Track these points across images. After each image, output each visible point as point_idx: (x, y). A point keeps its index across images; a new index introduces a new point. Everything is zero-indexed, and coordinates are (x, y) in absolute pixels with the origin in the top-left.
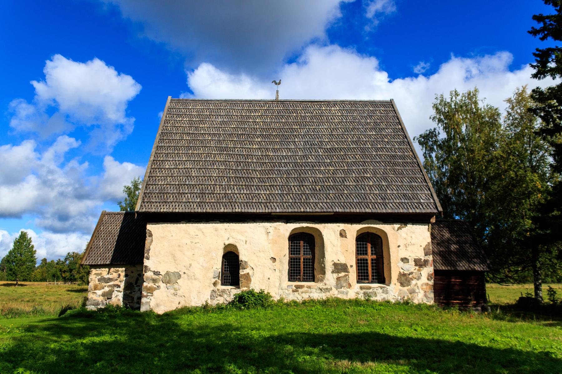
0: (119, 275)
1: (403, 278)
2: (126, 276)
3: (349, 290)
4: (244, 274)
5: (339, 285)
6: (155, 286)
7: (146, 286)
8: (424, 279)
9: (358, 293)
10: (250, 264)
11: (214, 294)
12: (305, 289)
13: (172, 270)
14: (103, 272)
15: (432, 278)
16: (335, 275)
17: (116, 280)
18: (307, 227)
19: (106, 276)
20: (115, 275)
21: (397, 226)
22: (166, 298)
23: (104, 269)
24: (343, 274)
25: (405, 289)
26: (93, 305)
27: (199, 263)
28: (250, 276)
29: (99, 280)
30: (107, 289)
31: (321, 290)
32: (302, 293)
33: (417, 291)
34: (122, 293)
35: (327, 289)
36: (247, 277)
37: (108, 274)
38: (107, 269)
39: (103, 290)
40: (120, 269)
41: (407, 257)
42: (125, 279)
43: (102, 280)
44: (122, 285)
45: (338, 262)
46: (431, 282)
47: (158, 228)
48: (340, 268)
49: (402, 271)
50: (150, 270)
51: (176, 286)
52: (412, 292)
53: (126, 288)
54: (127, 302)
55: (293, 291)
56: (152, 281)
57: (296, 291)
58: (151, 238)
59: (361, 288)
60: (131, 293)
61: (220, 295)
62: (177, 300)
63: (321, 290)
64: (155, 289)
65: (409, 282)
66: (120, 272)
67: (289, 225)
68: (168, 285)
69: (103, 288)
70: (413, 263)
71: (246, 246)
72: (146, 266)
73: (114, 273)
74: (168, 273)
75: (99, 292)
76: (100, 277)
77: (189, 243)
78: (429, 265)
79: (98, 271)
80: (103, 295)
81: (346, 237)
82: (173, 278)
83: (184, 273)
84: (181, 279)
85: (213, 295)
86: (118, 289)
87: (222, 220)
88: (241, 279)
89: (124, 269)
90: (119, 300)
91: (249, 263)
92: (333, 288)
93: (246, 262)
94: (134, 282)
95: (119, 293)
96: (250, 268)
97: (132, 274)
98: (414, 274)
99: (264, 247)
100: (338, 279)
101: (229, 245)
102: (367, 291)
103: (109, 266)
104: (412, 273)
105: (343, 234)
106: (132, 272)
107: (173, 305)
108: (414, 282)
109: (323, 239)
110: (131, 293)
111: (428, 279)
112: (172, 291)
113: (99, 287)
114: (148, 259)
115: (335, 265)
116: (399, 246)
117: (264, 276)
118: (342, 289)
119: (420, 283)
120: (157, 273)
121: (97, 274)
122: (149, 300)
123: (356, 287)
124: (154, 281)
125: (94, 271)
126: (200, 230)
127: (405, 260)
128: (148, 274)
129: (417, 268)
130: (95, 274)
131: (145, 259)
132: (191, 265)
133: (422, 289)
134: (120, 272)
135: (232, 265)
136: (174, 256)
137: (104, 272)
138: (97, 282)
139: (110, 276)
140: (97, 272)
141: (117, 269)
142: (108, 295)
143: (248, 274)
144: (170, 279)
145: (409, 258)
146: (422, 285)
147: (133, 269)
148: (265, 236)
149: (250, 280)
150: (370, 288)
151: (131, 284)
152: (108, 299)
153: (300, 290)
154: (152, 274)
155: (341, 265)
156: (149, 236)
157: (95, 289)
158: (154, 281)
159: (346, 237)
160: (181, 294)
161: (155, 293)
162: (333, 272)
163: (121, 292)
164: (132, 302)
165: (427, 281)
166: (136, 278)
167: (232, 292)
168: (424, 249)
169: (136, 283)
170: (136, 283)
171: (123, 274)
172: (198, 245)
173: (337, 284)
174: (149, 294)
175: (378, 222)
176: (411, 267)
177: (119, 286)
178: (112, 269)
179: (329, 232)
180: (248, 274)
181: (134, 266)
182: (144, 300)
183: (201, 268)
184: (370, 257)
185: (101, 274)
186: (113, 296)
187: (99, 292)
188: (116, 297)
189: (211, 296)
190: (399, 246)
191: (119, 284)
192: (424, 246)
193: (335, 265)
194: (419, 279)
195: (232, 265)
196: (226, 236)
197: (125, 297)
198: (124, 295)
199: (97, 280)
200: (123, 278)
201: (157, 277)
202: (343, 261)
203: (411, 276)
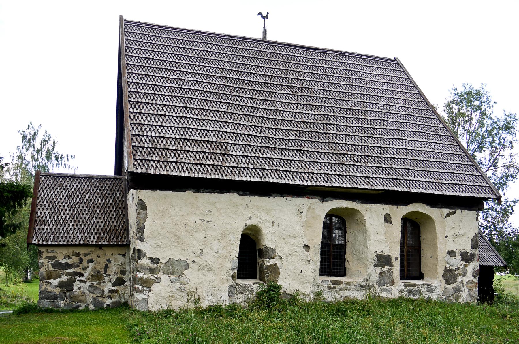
0: (81, 260)
1: (448, 275)
3: (392, 287)
4: (271, 265)
5: (381, 283)
6: (153, 278)
8: (469, 277)
9: (401, 291)
11: (232, 290)
12: (344, 285)
14: (57, 256)
15: (477, 275)
16: (378, 270)
17: (78, 266)
18: (347, 208)
21: (446, 211)
24: (386, 268)
25: (451, 287)
27: (212, 249)
29: (53, 266)
30: (65, 278)
31: (362, 287)
32: (340, 290)
33: (462, 289)
35: (369, 285)
36: (274, 269)
41: (454, 250)
43: (58, 265)
45: (382, 253)
46: (476, 280)
47: (306, 225)
48: (383, 260)
49: (448, 266)
50: (145, 256)
51: (183, 279)
52: (457, 290)
55: (330, 288)
56: (148, 271)
57: (334, 288)
58: (144, 212)
59: (406, 286)
60: (99, 284)
61: (241, 292)
64: (154, 282)
65: (454, 278)
67: (325, 203)
68: (172, 277)
69: (60, 277)
70: (460, 257)
71: (272, 229)
73: (73, 257)
75: (55, 282)
76: (54, 261)
77: (199, 221)
78: (476, 260)
80: (61, 285)
81: (391, 223)
82: (178, 268)
83: (194, 261)
84: (189, 270)
85: (232, 290)
87: (241, 193)
91: (277, 251)
92: (375, 285)
93: (273, 250)
94: (102, 270)
96: (278, 257)
97: (98, 260)
98: (460, 270)
99: (292, 232)
100: (381, 274)
101: (252, 226)
102: (411, 288)
104: (458, 269)
105: (388, 219)
106: (99, 257)
108: (460, 279)
110: (99, 284)
111: (473, 276)
113: (54, 275)
115: (379, 256)
116: (446, 237)
118: (385, 287)
119: (465, 280)
120: (155, 261)
121: (50, 258)
122: (146, 297)
123: (400, 284)
124: (152, 271)
127: (452, 253)
129: (464, 263)
130: (47, 257)
132: (202, 250)
133: (467, 287)
135: (251, 254)
136: (178, 238)
138: (51, 269)
143: (276, 264)
144: (175, 269)
145: (457, 251)
146: (467, 283)
149: (278, 273)
150: (415, 285)
152: (68, 291)
153: (338, 287)
154: (149, 261)
155: (384, 256)
158: (152, 271)
159: (391, 223)
162: (375, 266)
164: (102, 296)
165: (472, 278)
166: (104, 264)
168: (472, 241)
169: (105, 272)
172: (211, 224)
173: (380, 281)
174: (146, 289)
176: (457, 262)
179: (372, 214)
180: (276, 264)
184: (336, 234)
185: (55, 257)
187: (55, 282)
188: (79, 288)
189: (229, 293)
190: (446, 237)
192: (471, 238)
193: (379, 256)
194: (464, 275)
195: (251, 254)
196: (248, 214)
199: (50, 266)
201: (155, 266)
202: (387, 253)
203: (457, 272)
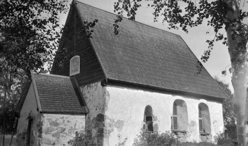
0: (64, 121)
138: (49, 126)
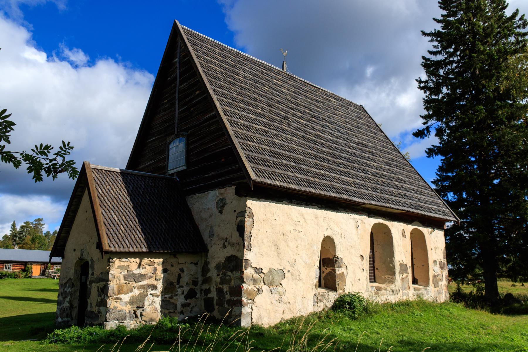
2: (165, 271)
7: (247, 289)
10: (346, 261)
13: (276, 267)
16: (401, 276)
17: (151, 277)
19: (137, 271)
20: (147, 270)
22: (269, 307)
23: (132, 260)
26: (117, 320)
28: (344, 276)
29: (125, 277)
30: (137, 292)
34: (160, 298)
37: (139, 267)
38: (138, 260)
39: (131, 294)
40: (157, 260)
42: (162, 275)
44: (160, 286)
48: (403, 268)
53: (165, 291)
54: (167, 311)
60: (171, 298)
62: (281, 307)
63: (393, 291)
66: (156, 265)
69: (131, 291)
72: (247, 260)
73: (147, 267)
74: (271, 271)
75: (126, 298)
76: (126, 272)
79: (125, 262)
82: (277, 278)
83: (289, 271)
84: (285, 279)
85: (317, 299)
86: (153, 292)
88: (337, 280)
89: (161, 260)
90: (156, 309)
94: (175, 281)
95: (156, 299)
101: (328, 236)
103: (140, 255)
106: (172, 266)
107: (278, 315)
109: (391, 238)
112: (277, 296)
113: (125, 289)
114: (250, 250)
117: (355, 276)
120: (259, 271)
125: (117, 262)
126: (302, 215)
128: (248, 272)
131: (245, 250)
134: (156, 265)
136: (277, 246)
137: (133, 262)
138: (123, 281)
139: (142, 271)
140: (122, 264)
141: (152, 260)
142: (138, 304)
143: (343, 273)
147: (173, 260)
148: (354, 230)
151: (172, 283)
156: (249, 217)
157: (119, 293)
160: (287, 301)
161: (258, 299)
163: (158, 296)
166: (177, 274)
167: (333, 297)
169: (178, 283)
170: (178, 283)
171: (160, 268)
172: (301, 234)
175: (420, 224)
177: (154, 287)
178: (145, 260)
180: (343, 273)
181: (175, 256)
182: (246, 310)
183: (304, 264)
186: (146, 303)
187: (126, 298)
188: (152, 304)
191: (155, 283)
197: (165, 304)
198: (163, 301)
199: (122, 278)
200: (160, 275)
